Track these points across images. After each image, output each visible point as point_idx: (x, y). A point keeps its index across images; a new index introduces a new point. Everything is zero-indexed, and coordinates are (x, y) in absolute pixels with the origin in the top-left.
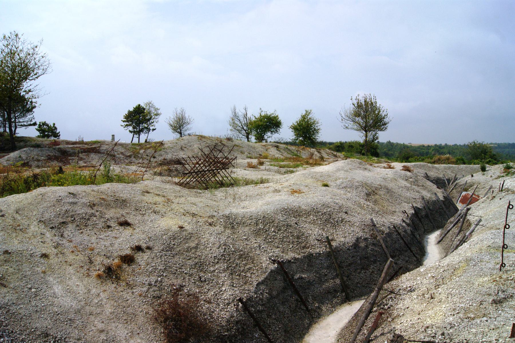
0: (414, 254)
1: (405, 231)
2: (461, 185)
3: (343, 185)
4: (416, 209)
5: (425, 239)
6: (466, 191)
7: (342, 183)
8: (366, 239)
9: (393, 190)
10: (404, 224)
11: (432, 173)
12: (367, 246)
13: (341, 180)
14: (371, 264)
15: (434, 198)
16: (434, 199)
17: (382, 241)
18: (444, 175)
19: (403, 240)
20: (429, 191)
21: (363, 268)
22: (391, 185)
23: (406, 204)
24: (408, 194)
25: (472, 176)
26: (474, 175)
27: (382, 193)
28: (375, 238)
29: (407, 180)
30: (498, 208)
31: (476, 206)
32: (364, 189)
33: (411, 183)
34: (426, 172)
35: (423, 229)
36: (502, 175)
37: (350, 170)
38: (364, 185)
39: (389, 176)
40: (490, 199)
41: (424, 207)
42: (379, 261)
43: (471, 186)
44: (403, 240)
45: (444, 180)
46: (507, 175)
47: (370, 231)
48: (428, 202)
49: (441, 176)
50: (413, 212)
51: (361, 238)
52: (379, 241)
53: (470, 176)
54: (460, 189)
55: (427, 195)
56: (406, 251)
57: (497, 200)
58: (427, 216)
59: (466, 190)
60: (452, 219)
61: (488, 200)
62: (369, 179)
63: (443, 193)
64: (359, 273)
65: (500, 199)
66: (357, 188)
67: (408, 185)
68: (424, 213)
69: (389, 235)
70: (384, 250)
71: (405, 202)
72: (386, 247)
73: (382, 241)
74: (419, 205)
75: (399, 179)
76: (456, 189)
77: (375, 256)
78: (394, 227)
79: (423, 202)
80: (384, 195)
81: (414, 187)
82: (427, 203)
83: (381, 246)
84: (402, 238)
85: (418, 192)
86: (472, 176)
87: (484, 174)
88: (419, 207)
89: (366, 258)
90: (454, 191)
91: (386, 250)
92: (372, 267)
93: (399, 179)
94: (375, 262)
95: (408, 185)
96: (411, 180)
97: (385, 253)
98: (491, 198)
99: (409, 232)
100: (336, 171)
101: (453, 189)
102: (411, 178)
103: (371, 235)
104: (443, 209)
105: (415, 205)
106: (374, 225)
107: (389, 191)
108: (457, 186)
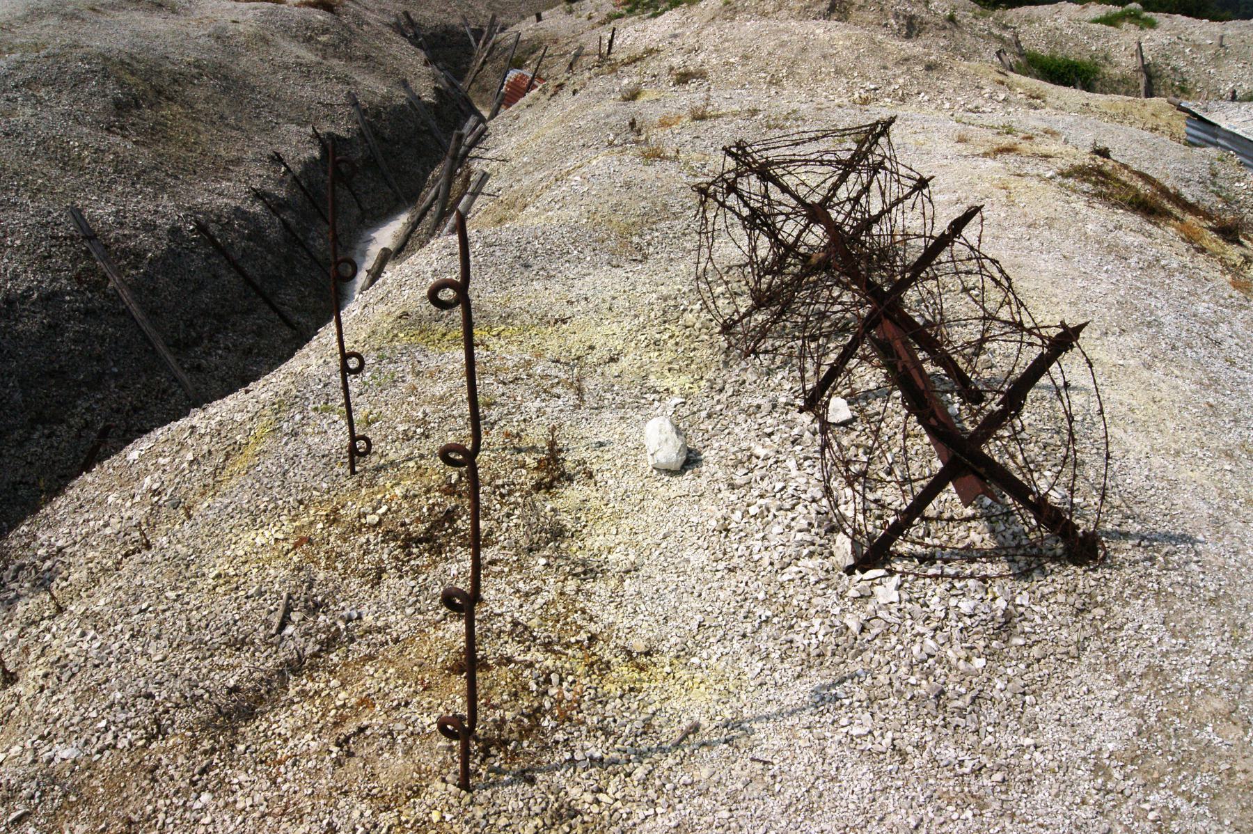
0: (282, 316)
1: (257, 234)
2: (506, 49)
3: (20, 76)
4: (330, 144)
5: (360, 246)
6: (520, 67)
7: (20, 65)
8: (50, 298)
9: (251, 80)
10: (258, 208)
11: (428, 14)
12: (55, 328)
13: (17, 56)
14: (79, 396)
15: (400, 96)
16: (402, 101)
17: (126, 295)
18: (463, 17)
19: (241, 271)
20: (385, 76)
21: (39, 419)
22: (247, 62)
23: (294, 128)
24: (308, 92)
25: (539, 18)
26: (543, 14)
27: (200, 93)
28: (99, 286)
29: (309, 40)
30: (556, 124)
31: (507, 121)
32: (110, 84)
33: (324, 50)
34: (404, 7)
35: (356, 211)
36: (620, 10)
37: (87, 14)
38: (108, 66)
39: (241, 28)
40: (549, 94)
41: (361, 134)
42: (116, 376)
43: (534, 50)
44: (241, 271)
45: (465, 35)
46: (630, 11)
47: (74, 261)
48: (378, 115)
49: (456, 21)
50: (317, 154)
51: (25, 297)
52: (115, 297)
53: (534, 17)
54: (502, 62)
55: (374, 87)
56: (249, 311)
57: (565, 95)
58: (370, 162)
59: (518, 64)
60: (437, 171)
61: (543, 98)
62: (158, 41)
63: (436, 80)
64: (20, 444)
65: (575, 92)
66: (79, 80)
67: (309, 56)
68: (358, 154)
69: (172, 260)
70: (140, 330)
71: (291, 121)
72: (152, 313)
73: (126, 295)
74: (342, 129)
75: (278, 38)
76: (492, 61)
77: (99, 359)
78: (201, 228)
79: (357, 116)
80: (207, 100)
81: (335, 62)
82: (373, 119)
83: (126, 312)
84: (234, 265)
85: (345, 80)
86: (539, 18)
87: (570, 12)
88: (343, 134)
89: (51, 374)
90: (488, 67)
91: (146, 327)
92: (82, 405)
93: (278, 38)
94: (97, 382)
95: (309, 56)
96: (323, 38)
97: (146, 339)
98: (551, 90)
99: (273, 234)
100: (24, 19)
101: (484, 62)
102: (326, 31)
103: (78, 277)
104: (430, 132)
105: (326, 128)
106: (91, 236)
107: (232, 85)
108: (495, 53)
